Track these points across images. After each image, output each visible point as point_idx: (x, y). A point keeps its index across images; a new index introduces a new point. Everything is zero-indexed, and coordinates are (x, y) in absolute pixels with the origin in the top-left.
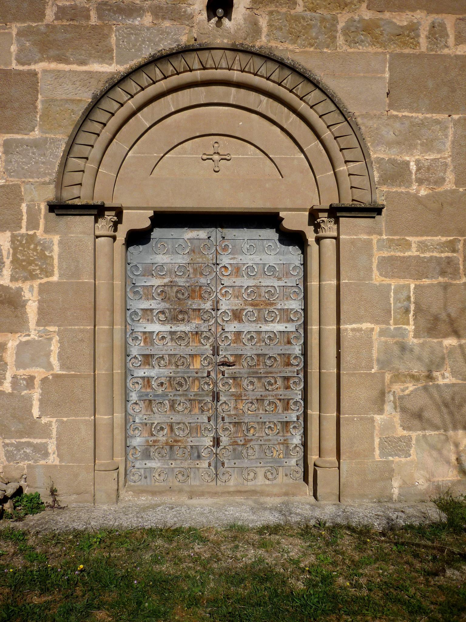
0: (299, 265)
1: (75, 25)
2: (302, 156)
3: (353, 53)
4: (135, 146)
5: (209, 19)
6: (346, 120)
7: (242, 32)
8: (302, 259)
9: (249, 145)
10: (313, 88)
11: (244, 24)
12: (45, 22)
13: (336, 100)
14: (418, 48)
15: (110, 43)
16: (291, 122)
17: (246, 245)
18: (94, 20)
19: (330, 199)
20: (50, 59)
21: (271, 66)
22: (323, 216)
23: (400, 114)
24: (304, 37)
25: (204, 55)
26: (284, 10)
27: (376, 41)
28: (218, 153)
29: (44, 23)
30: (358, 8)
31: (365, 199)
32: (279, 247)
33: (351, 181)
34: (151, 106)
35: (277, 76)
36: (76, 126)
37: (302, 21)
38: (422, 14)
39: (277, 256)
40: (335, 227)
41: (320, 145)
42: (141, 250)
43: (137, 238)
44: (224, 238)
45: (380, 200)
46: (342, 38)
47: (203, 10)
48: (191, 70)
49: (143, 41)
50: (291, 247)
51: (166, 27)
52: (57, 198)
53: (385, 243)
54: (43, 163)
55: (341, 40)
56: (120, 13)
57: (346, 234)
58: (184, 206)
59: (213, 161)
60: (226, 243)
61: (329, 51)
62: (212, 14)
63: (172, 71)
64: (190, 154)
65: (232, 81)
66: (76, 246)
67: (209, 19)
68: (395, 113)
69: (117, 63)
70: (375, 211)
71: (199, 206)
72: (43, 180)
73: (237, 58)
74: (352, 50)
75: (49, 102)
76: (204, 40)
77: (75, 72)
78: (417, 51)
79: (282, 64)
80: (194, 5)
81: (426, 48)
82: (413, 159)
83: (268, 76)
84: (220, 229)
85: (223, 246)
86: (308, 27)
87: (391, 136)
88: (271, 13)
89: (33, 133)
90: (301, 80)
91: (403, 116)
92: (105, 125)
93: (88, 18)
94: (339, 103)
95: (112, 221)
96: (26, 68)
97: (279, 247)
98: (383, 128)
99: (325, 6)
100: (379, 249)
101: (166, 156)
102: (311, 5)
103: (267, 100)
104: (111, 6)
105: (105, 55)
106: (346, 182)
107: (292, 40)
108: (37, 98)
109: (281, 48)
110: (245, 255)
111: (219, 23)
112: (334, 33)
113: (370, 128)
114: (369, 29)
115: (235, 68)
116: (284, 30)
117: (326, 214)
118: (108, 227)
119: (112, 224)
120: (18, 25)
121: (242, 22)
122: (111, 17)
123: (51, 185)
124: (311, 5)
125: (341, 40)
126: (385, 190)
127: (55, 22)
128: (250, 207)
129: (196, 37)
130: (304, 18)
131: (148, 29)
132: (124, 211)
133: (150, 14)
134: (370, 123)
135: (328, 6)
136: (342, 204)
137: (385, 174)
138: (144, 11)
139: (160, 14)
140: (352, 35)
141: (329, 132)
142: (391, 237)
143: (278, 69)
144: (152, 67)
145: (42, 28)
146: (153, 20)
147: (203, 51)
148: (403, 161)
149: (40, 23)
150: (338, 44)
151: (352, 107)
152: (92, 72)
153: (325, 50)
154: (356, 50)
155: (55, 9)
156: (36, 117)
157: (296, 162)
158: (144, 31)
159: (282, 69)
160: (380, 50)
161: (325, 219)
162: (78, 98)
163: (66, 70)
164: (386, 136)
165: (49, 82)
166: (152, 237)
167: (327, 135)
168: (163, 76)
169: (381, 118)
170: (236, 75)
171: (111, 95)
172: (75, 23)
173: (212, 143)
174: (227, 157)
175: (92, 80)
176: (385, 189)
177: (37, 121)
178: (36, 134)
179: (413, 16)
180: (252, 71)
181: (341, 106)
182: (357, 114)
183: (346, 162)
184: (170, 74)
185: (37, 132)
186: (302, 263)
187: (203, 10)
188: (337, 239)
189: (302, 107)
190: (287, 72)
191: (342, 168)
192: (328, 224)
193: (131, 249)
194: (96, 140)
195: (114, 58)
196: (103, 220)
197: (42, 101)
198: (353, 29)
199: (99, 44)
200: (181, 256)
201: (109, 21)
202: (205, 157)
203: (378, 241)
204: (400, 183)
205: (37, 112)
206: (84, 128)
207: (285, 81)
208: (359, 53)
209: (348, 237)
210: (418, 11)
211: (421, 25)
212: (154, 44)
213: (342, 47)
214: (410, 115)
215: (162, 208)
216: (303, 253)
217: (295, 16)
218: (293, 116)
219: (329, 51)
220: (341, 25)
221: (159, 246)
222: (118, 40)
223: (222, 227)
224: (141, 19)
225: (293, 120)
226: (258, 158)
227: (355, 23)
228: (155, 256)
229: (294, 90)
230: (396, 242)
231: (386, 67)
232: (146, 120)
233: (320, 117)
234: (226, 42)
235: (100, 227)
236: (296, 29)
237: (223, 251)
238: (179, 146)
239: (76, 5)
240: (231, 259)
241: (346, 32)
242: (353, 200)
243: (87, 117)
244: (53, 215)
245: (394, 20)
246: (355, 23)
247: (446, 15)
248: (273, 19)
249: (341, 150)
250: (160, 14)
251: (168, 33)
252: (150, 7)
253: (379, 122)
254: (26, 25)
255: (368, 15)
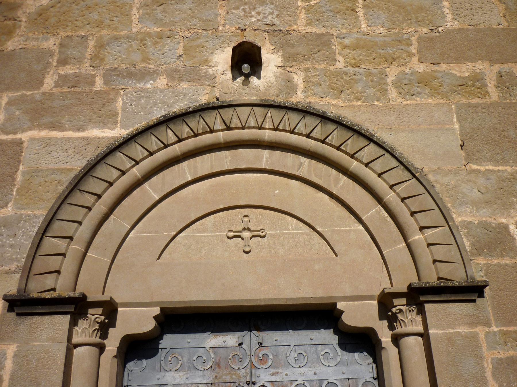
0: (372, 380)
1: (76, 92)
2: (361, 227)
3: (410, 105)
4: (140, 224)
5: (234, 78)
6: (414, 176)
7: (273, 89)
8: (375, 370)
9: (289, 218)
10: (366, 142)
11: (276, 81)
12: (42, 90)
13: (398, 155)
14: (487, 97)
15: (116, 107)
16: (342, 185)
17: (293, 353)
18: (99, 84)
19: (404, 279)
20: (40, 127)
21: (311, 122)
22: (400, 303)
23: (483, 168)
24: (349, 91)
25: (227, 113)
26: (322, 66)
27: (435, 92)
28: (249, 229)
29: (41, 91)
30: (408, 62)
31: (457, 276)
32: (339, 353)
33: (431, 253)
34: (161, 175)
35: (320, 133)
36: (59, 197)
37: (344, 76)
38: (484, 64)
39: (339, 368)
40: (419, 318)
41: (383, 211)
42: (144, 366)
43: (138, 348)
44: (261, 344)
45: (479, 277)
46: (394, 91)
47: (227, 70)
48: (212, 131)
49: (155, 104)
50: (356, 355)
51: (183, 88)
52: (19, 290)
53: (497, 338)
54: (12, 246)
55: (393, 93)
56: (130, 78)
57: (438, 327)
58: (203, 298)
59: (243, 239)
60: (265, 352)
61: (381, 104)
62: (237, 73)
63: (188, 132)
64: (212, 232)
65: (264, 141)
66: (38, 360)
67: (234, 78)
68: (475, 167)
69: (122, 127)
70: (472, 291)
71: (223, 299)
72: (7, 268)
73: (269, 115)
74: (408, 102)
75: (32, 173)
76: (228, 99)
77: (69, 139)
78: (487, 100)
79: (324, 118)
80: (216, 66)
81: (497, 97)
82: (512, 221)
83: (308, 132)
84: (255, 332)
85: (260, 355)
86: (352, 81)
87: (476, 195)
88: (307, 70)
89: (5, 209)
90: (350, 134)
91: (486, 170)
92: (99, 196)
93: (93, 83)
94: (402, 157)
95: (98, 323)
96: (10, 137)
97: (339, 353)
98: (463, 185)
99: (369, 60)
100: (491, 347)
101: (181, 235)
102: (354, 61)
103: (309, 162)
104: (119, 71)
105: (109, 119)
106: (425, 256)
107: (334, 95)
108: (18, 169)
109: (322, 103)
110: (292, 369)
111: (246, 83)
112: (384, 86)
113: (447, 185)
114: (424, 81)
115: (267, 127)
116: (323, 86)
117: (404, 301)
118: (91, 331)
119: (97, 326)
120: (10, 94)
121: (273, 79)
122: (119, 81)
123: (17, 275)
124: (354, 61)
125: (393, 93)
126: (482, 262)
127: (54, 89)
128: (295, 297)
129: (218, 96)
130: (346, 74)
131: (162, 91)
132: (120, 309)
133: (165, 77)
134: (446, 180)
135: (373, 61)
136: (426, 283)
137: (478, 241)
138: (157, 74)
139: (177, 76)
140: (406, 87)
141: (393, 193)
142: (505, 329)
143: (320, 125)
144: (163, 128)
145: (38, 96)
146: (168, 82)
147: (227, 109)
148: (500, 224)
149: (36, 92)
150: (390, 97)
151: (417, 162)
152: (91, 138)
153: (375, 103)
154: (413, 102)
155: (56, 77)
156: (12, 190)
157: (353, 236)
158: (157, 93)
159: (325, 123)
160: (442, 101)
161: (403, 308)
162: (69, 167)
163: (59, 137)
164: (469, 194)
165: (35, 151)
166: (161, 346)
167: (390, 197)
168: (177, 139)
169: (459, 173)
170: (268, 135)
171: (110, 160)
172: (77, 89)
173: (240, 216)
174: (260, 233)
175: (89, 146)
176: (482, 261)
177: (12, 195)
178: (10, 210)
179: (474, 67)
180: (288, 129)
181: (404, 161)
182: (426, 170)
183: (422, 229)
184: (186, 136)
185: (10, 209)
186: (375, 376)
187: (227, 70)
188: (425, 336)
189: (354, 166)
190: (331, 127)
191: (417, 237)
192: (408, 314)
193: (130, 365)
194: (86, 215)
195: (119, 122)
196: (85, 322)
197: (23, 173)
198: (406, 82)
199: (102, 109)
200: (200, 373)
201: (116, 86)
202: (231, 234)
203: (487, 334)
204: (501, 252)
205: (15, 185)
206: (69, 200)
207: (330, 138)
208: (417, 105)
209: (441, 332)
210: (479, 62)
211: (485, 75)
212: (168, 106)
213: (396, 100)
214: (496, 168)
215: (171, 302)
216: (375, 361)
217: (335, 72)
218: (344, 179)
219: (381, 104)
220: (390, 79)
221: (170, 359)
222: (124, 103)
223: (259, 330)
224: (154, 82)
225: (344, 183)
226: (302, 233)
227: (407, 76)
228: (163, 373)
229: (342, 147)
230: (514, 335)
231: (453, 118)
232: (155, 191)
233: (379, 175)
234: (254, 99)
235: (80, 331)
236: (339, 86)
237: (261, 363)
238: (198, 223)
239: (81, 73)
240: (272, 374)
241: (398, 84)
242: (439, 278)
243: (75, 186)
244: (13, 315)
245: (453, 72)
246: (407, 76)
247: (513, 64)
248: (310, 75)
249: (413, 214)
250: (177, 76)
251: (185, 95)
252: (165, 70)
253: (457, 178)
254: (19, 94)
255: (421, 68)
